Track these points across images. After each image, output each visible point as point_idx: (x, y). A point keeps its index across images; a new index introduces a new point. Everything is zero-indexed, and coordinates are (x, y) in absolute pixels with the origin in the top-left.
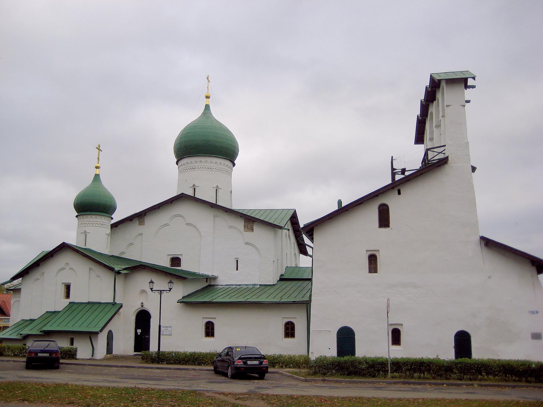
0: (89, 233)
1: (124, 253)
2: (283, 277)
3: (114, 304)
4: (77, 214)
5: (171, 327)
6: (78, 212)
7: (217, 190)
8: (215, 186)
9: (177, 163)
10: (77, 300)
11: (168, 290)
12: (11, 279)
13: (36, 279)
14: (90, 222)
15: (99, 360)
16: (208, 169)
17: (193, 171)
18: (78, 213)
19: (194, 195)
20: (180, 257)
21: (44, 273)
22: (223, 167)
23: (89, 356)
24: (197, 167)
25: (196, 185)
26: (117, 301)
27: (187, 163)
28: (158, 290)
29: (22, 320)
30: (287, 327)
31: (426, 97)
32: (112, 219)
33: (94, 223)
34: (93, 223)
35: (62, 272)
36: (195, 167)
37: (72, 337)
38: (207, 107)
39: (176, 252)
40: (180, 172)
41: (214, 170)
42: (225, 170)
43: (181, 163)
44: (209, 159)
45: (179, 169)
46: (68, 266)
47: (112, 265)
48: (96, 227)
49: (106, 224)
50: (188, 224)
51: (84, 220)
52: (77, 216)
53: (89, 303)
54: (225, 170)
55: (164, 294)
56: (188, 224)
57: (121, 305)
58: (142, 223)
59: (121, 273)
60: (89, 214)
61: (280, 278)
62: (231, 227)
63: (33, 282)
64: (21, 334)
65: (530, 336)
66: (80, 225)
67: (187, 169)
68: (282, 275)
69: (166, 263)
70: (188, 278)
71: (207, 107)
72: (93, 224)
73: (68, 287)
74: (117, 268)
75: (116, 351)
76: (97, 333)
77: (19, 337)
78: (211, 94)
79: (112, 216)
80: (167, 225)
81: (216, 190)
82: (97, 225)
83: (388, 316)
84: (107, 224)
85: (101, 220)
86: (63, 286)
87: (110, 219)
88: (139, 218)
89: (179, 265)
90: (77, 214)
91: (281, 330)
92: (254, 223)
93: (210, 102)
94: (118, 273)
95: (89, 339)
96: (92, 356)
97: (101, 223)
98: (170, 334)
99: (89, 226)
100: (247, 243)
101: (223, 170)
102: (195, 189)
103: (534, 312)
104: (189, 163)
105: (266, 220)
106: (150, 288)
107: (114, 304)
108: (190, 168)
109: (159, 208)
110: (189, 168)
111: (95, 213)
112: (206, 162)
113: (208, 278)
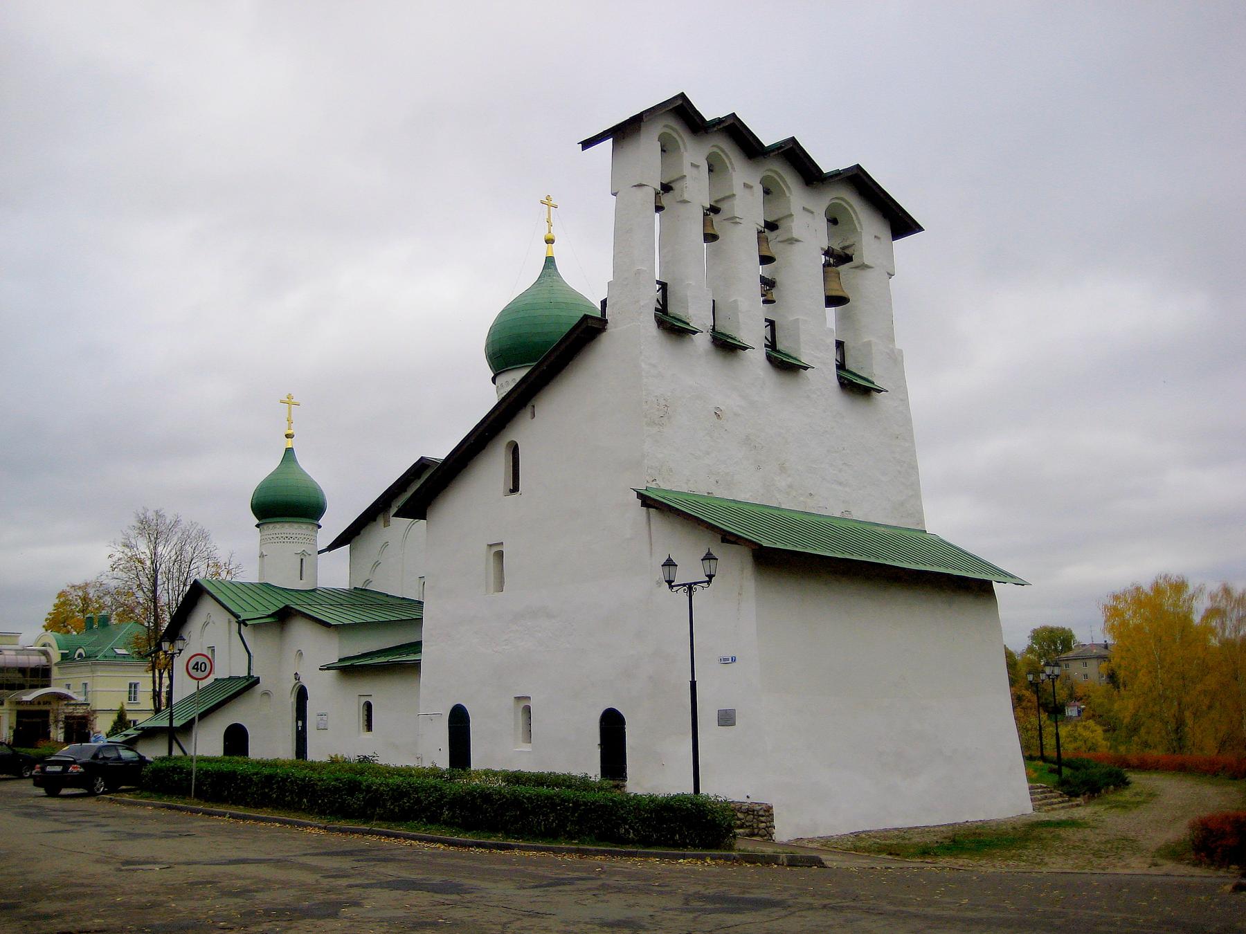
4: (257, 522)
11: (704, 582)
26: (255, 674)
28: (684, 585)
31: (870, 183)
32: (320, 527)
34: (280, 536)
38: (550, 261)
43: (499, 380)
48: (282, 544)
52: (258, 526)
53: (230, 678)
55: (698, 593)
60: (277, 522)
71: (550, 261)
78: (555, 233)
79: (320, 522)
81: (302, 560)
87: (315, 528)
93: (556, 251)
106: (666, 581)
107: (250, 676)
111: (275, 519)
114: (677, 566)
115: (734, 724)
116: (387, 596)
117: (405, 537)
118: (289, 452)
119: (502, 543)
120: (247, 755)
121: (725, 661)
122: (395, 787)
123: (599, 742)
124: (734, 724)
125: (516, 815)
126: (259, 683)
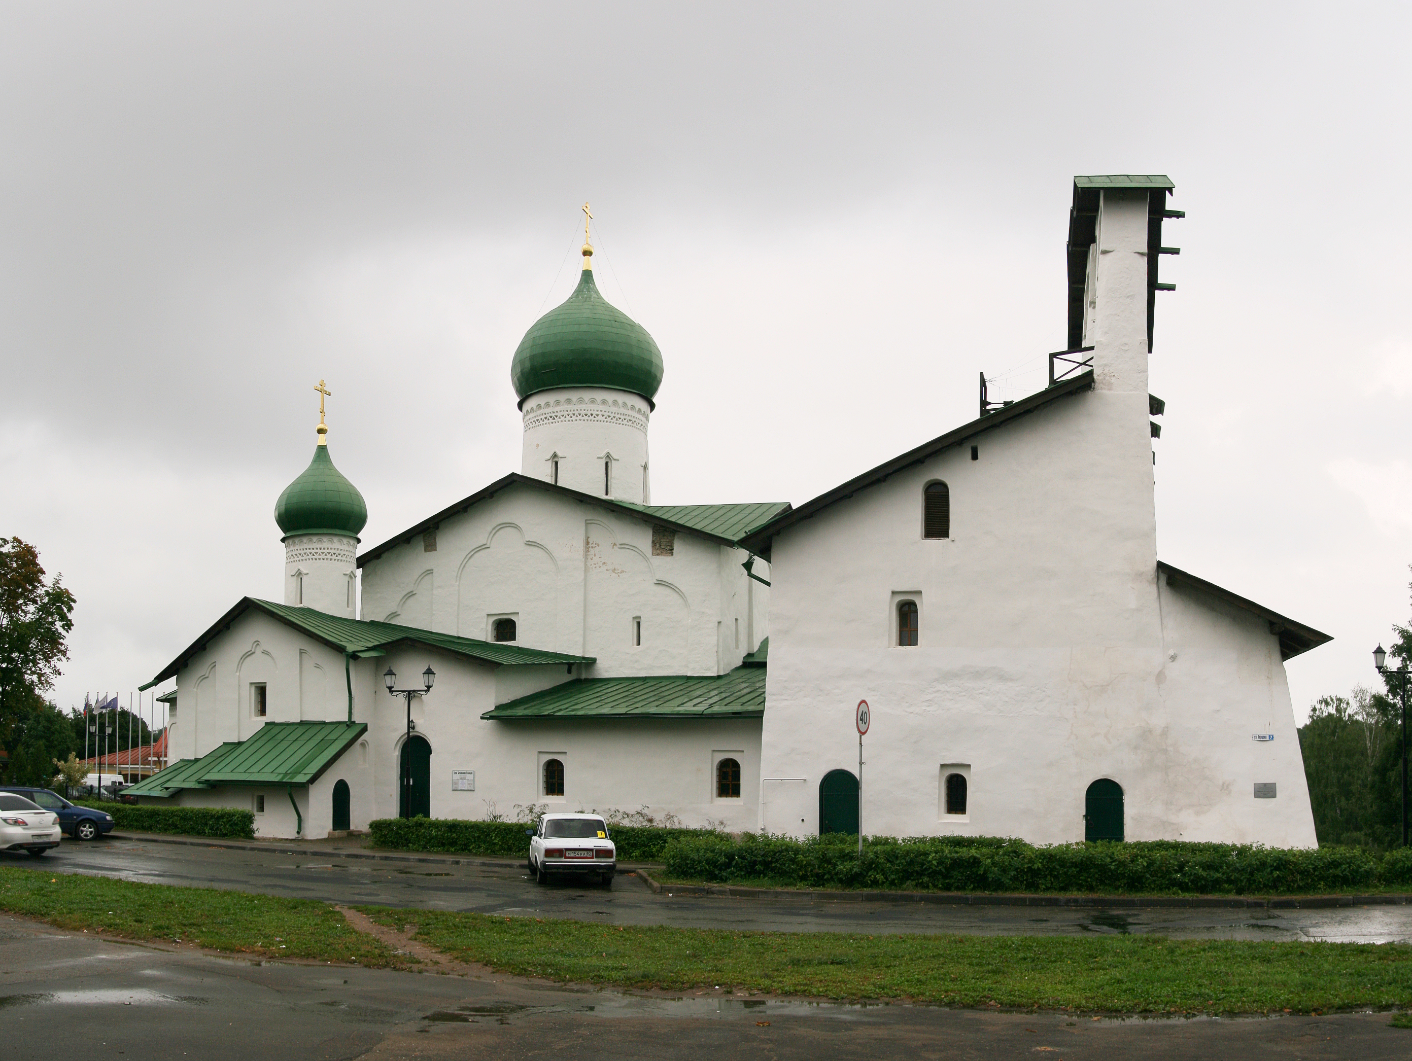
0: (308, 574)
1: (395, 614)
2: (751, 660)
3: (350, 724)
4: (283, 535)
5: (472, 773)
6: (285, 531)
7: (609, 464)
8: (603, 454)
9: (520, 406)
10: (278, 719)
12: (156, 678)
13: (200, 677)
14: (308, 551)
15: (311, 841)
16: (586, 418)
17: (552, 423)
18: (285, 532)
19: (556, 481)
20: (513, 618)
21: (214, 664)
22: (622, 410)
23: (292, 835)
24: (559, 414)
25: (560, 454)
26: (357, 718)
27: (539, 406)
28: (404, 691)
29: (182, 760)
30: (724, 772)
32: (359, 541)
33: (316, 553)
34: (313, 552)
35: (247, 660)
36: (556, 414)
37: (261, 794)
38: (587, 276)
39: (503, 608)
40: (527, 428)
41: (600, 418)
42: (628, 418)
44: (587, 395)
45: (525, 420)
46: (258, 646)
47: (343, 639)
49: (342, 553)
50: (529, 544)
51: (311, 547)
52: (283, 540)
53: (302, 723)
54: (628, 418)
56: (529, 544)
57: (362, 727)
58: (431, 546)
59: (359, 657)
61: (743, 662)
62: (623, 546)
63: (198, 683)
64: (167, 788)
65: (1251, 790)
66: (292, 557)
67: (592, 415)
68: (750, 655)
69: (483, 632)
70: (503, 664)
71: (587, 276)
72: (314, 555)
73: (262, 691)
74: (351, 648)
75: (360, 820)
76: (303, 788)
77: (164, 794)
79: (360, 536)
80: (484, 547)
81: (607, 463)
82: (323, 556)
83: (861, 741)
84: (345, 553)
85: (330, 546)
86: (253, 689)
88: (424, 537)
89: (513, 637)
90: (283, 535)
91: (709, 779)
92: (674, 536)
94: (354, 656)
95: (289, 799)
96: (298, 833)
97: (332, 551)
98: (470, 788)
99: (306, 559)
100: (660, 583)
101: (622, 417)
102: (556, 463)
103: (1265, 737)
104: (542, 405)
105: (708, 530)
106: (387, 687)
107: (350, 724)
108: (545, 416)
109: (466, 511)
110: (543, 417)
112: (581, 401)
113: (573, 664)
114: (435, 674)
115: (1274, 796)
116: (431, 633)
117: (463, 566)
118: (322, 449)
119: (518, 613)
120: (429, 817)
121: (1262, 739)
122: (723, 859)
123: (1084, 813)
124: (1274, 796)
125: (1026, 885)
126: (367, 730)
